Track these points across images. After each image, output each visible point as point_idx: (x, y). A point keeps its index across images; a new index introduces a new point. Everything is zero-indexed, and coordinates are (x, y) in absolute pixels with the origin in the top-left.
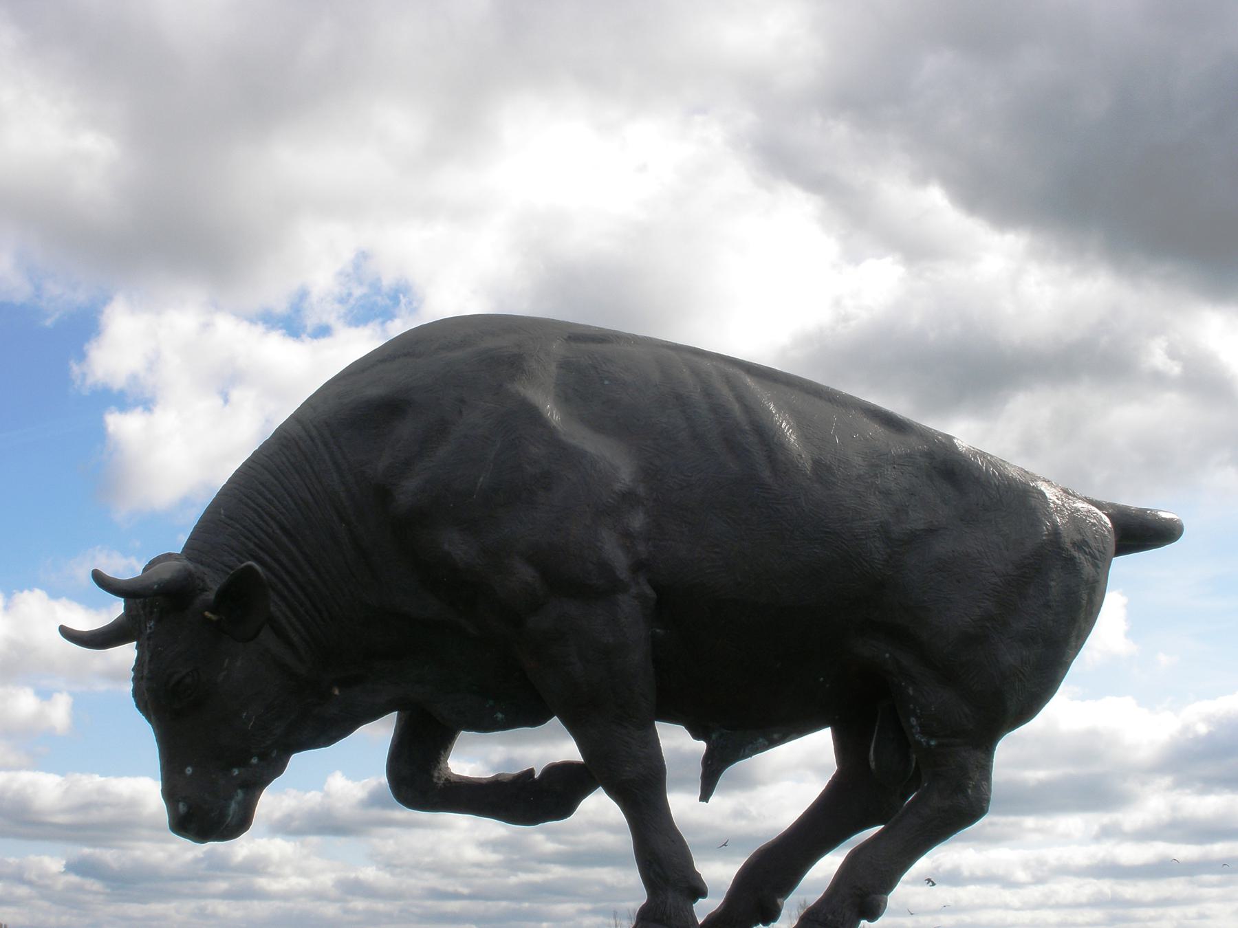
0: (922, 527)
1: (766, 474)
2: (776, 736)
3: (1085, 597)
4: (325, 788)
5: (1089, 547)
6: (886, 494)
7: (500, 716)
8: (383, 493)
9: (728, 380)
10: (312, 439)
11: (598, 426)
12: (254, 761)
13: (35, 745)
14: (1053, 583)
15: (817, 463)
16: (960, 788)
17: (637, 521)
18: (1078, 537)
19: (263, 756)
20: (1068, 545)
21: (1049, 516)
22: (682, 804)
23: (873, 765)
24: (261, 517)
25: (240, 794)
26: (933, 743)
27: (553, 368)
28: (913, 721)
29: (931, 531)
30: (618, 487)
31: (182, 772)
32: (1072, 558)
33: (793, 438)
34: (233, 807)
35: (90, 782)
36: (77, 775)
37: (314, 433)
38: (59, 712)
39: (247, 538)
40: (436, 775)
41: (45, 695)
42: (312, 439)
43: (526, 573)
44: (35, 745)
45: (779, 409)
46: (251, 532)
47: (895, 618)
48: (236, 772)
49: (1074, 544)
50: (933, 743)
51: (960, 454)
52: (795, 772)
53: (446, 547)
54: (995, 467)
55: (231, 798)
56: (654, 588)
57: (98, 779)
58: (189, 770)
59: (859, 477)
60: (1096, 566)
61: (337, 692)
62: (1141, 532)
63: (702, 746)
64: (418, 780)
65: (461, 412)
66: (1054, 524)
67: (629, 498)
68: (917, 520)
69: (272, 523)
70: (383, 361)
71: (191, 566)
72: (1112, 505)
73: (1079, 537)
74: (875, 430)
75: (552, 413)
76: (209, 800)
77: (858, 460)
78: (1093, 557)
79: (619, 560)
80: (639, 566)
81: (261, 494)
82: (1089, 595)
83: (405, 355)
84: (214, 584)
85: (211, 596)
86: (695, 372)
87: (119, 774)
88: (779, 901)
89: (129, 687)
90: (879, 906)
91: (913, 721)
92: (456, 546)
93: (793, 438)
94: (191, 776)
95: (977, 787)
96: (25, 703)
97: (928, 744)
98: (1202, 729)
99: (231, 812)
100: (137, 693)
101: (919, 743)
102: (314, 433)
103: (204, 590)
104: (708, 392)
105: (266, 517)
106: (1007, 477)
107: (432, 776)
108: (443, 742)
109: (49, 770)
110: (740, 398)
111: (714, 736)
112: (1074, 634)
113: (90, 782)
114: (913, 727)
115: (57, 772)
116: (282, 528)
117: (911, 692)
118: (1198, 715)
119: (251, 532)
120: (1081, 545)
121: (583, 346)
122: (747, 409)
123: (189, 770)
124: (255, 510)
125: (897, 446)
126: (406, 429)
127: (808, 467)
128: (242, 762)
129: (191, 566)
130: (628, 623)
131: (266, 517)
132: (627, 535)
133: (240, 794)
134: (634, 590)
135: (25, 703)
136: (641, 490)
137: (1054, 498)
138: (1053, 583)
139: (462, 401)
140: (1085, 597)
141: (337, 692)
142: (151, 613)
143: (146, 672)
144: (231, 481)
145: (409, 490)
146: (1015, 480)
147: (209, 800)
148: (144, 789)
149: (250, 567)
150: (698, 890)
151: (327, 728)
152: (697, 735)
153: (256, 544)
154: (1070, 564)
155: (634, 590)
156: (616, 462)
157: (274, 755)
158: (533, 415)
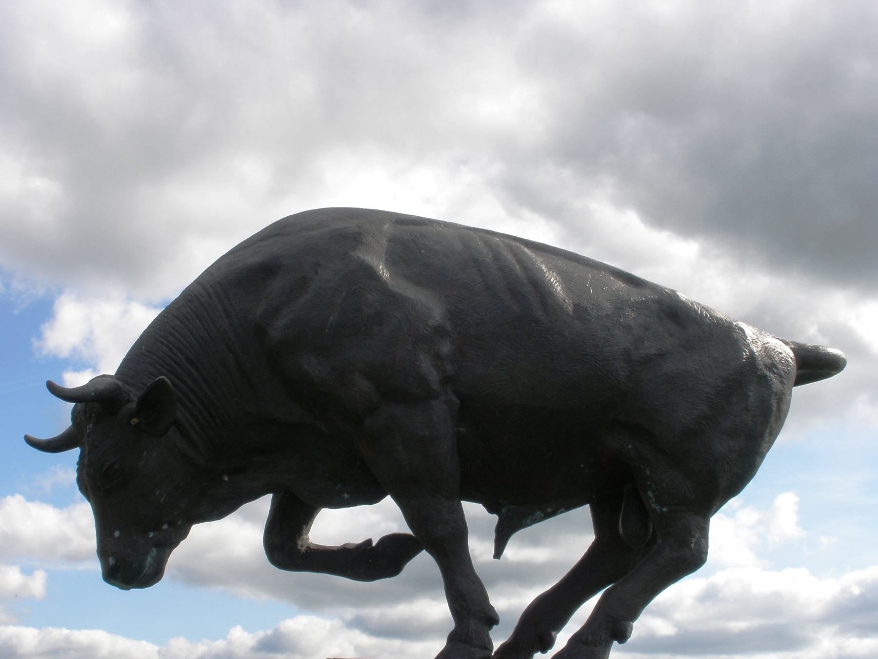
0: (654, 352)
1: (539, 313)
2: (549, 510)
3: (775, 404)
4: (228, 637)
5: (777, 368)
6: (627, 328)
7: (346, 496)
8: (260, 331)
9: (512, 250)
10: (209, 295)
11: (417, 281)
12: (165, 527)
13: (19, 607)
14: (751, 394)
15: (577, 306)
16: (685, 543)
17: (446, 348)
18: (768, 361)
19: (172, 524)
20: (762, 367)
21: (748, 346)
22: (480, 549)
23: (621, 531)
24: (171, 350)
25: (154, 552)
26: (665, 510)
27: (384, 242)
28: (650, 493)
29: (661, 355)
30: (431, 322)
31: (111, 534)
32: (765, 376)
33: (559, 289)
34: (149, 560)
35: (59, 633)
36: (50, 628)
37: (211, 290)
38: (38, 584)
39: (161, 365)
40: (300, 543)
41: (28, 571)
42: (209, 295)
43: (364, 386)
44: (19, 607)
45: (549, 269)
46: (164, 361)
47: (637, 432)
48: (151, 535)
49: (766, 366)
50: (665, 510)
51: (682, 301)
52: (563, 542)
53: (306, 367)
54: (707, 311)
55: (147, 553)
56: (458, 397)
57: (65, 631)
58: (117, 534)
59: (607, 316)
60: (782, 383)
61: (226, 478)
62: (815, 365)
63: (495, 518)
64: (285, 545)
65: (317, 272)
66: (752, 352)
67: (439, 331)
68: (650, 347)
69: (179, 354)
70: (261, 240)
71: (120, 383)
72: (793, 343)
73: (770, 361)
74: (621, 285)
75: (384, 272)
76: (133, 553)
77: (607, 305)
78: (781, 376)
79: (433, 377)
80: (446, 380)
81: (172, 335)
82: (778, 404)
83: (277, 235)
84: (135, 395)
85: (133, 405)
86: (487, 244)
87: (80, 628)
88: (553, 633)
89: (74, 476)
90: (627, 629)
91: (650, 493)
92: (313, 366)
93: (559, 289)
94: (120, 536)
95: (698, 543)
96: (13, 577)
97: (661, 511)
98: (856, 591)
99: (148, 564)
100: (80, 480)
101: (655, 510)
102: (211, 290)
103: (129, 401)
104: (497, 257)
105: (175, 351)
106: (716, 318)
107: (297, 544)
108: (306, 516)
109: (27, 625)
110: (520, 261)
111: (504, 511)
112: (768, 431)
113: (59, 633)
114: (650, 498)
115: (35, 627)
116: (188, 359)
117: (648, 472)
118: (852, 581)
119: (164, 361)
120: (772, 367)
121: (406, 227)
122: (525, 268)
123: (117, 534)
124: (167, 346)
125: (635, 296)
126: (277, 285)
127: (570, 309)
128: (156, 528)
129: (120, 383)
130: (439, 419)
131: (175, 351)
132: (437, 357)
133: (154, 552)
134: (443, 398)
135: (13, 577)
136: (448, 326)
137: (751, 334)
138: (751, 394)
139: (318, 264)
140: (775, 404)
141: (226, 478)
142: (90, 418)
143: (86, 461)
144: (150, 327)
145: (278, 328)
146: (722, 320)
147: (133, 553)
148: (77, 524)
149: (162, 380)
150: (491, 619)
151: (219, 507)
152: (491, 510)
153: (167, 369)
154: (763, 381)
155: (443, 398)
156: (432, 307)
157: (180, 523)
158: (371, 273)
